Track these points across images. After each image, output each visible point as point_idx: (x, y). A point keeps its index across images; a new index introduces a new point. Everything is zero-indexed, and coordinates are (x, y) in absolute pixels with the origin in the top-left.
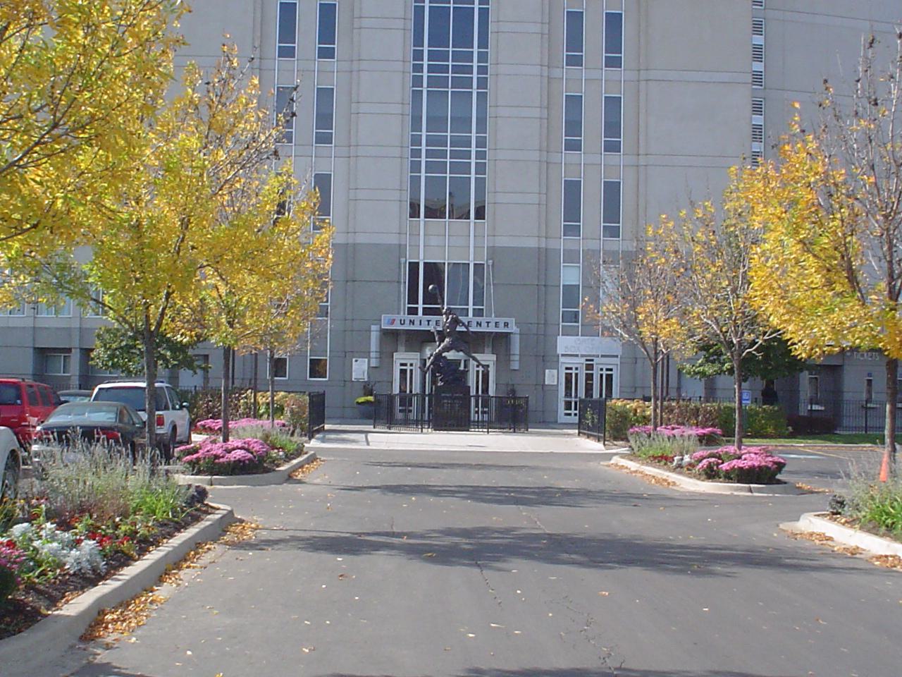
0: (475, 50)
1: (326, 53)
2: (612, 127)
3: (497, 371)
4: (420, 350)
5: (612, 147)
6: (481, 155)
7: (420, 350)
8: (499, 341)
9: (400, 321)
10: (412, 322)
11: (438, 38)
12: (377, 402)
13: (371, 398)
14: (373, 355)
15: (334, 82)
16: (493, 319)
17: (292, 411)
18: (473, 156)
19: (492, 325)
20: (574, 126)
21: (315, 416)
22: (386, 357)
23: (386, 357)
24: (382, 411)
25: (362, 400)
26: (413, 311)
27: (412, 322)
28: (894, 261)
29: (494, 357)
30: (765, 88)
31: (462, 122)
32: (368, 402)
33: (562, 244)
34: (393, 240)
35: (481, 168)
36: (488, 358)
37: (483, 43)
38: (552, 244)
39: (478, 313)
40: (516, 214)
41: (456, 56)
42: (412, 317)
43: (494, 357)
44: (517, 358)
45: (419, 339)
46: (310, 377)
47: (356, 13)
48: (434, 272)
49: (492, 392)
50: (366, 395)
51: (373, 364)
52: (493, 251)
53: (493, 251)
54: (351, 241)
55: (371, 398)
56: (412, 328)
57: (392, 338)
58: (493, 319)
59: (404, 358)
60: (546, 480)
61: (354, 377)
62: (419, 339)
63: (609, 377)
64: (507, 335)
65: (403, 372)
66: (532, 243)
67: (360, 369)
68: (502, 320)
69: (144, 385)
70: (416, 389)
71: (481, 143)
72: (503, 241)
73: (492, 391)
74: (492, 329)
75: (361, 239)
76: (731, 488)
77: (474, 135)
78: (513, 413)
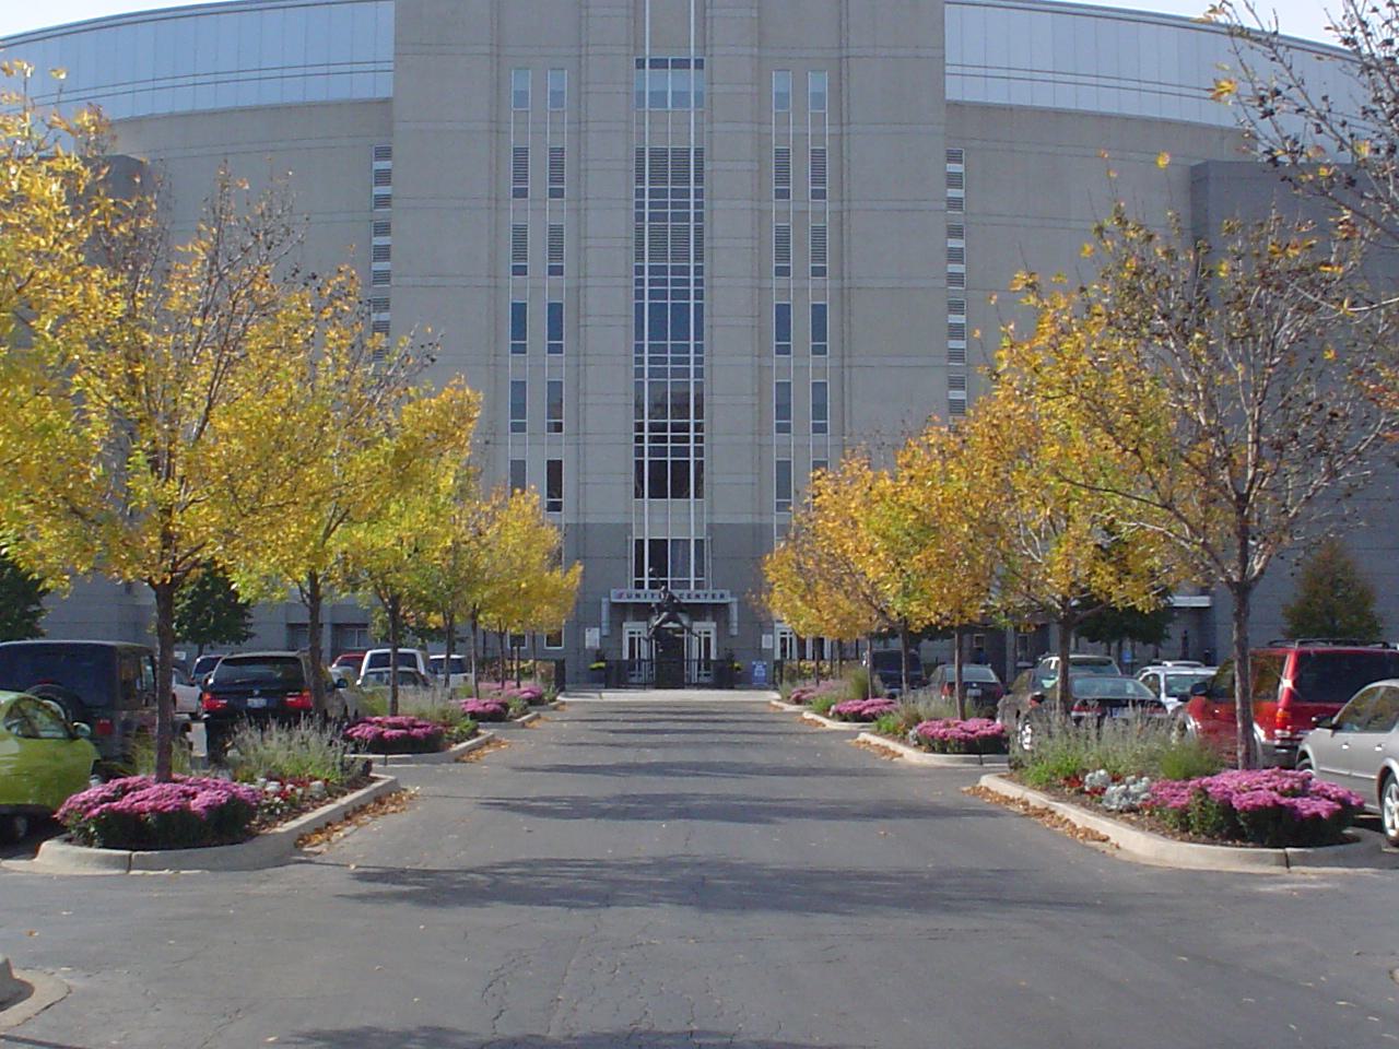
0: (692, 343)
1: (555, 350)
2: (819, 410)
3: (718, 639)
4: (647, 620)
5: (820, 429)
6: (699, 361)
7: (647, 620)
8: (718, 611)
9: (629, 595)
10: (638, 596)
11: (658, 331)
12: (609, 668)
13: (602, 664)
14: (604, 625)
15: (565, 376)
16: (711, 591)
17: (542, 674)
18: (692, 362)
19: (709, 596)
20: (783, 410)
21: (561, 681)
22: (616, 626)
23: (616, 626)
24: (614, 674)
25: (595, 666)
26: (640, 585)
27: (638, 596)
28: (1221, 495)
29: (714, 624)
30: (968, 365)
31: (658, 237)
32: (600, 668)
33: (775, 520)
34: (619, 520)
35: (699, 295)
36: (707, 626)
37: (699, 335)
38: (766, 520)
39: (698, 585)
40: (732, 491)
41: (664, 295)
42: (639, 591)
43: (714, 624)
44: (735, 625)
45: (643, 611)
46: (548, 645)
47: (582, 313)
48: (658, 547)
49: (713, 657)
50: (597, 661)
51: (605, 632)
52: (711, 527)
53: (711, 527)
54: (582, 522)
55: (602, 664)
56: (638, 600)
57: (621, 611)
58: (711, 591)
59: (631, 627)
60: (798, 805)
61: (587, 645)
62: (643, 611)
63: (707, 641)
64: (725, 606)
65: (632, 640)
66: (746, 519)
67: (592, 638)
68: (718, 593)
69: (443, 656)
70: (644, 656)
71: (699, 270)
72: (719, 519)
73: (713, 657)
74: (709, 600)
75: (590, 520)
76: (958, 760)
77: (692, 343)
78: (726, 675)
